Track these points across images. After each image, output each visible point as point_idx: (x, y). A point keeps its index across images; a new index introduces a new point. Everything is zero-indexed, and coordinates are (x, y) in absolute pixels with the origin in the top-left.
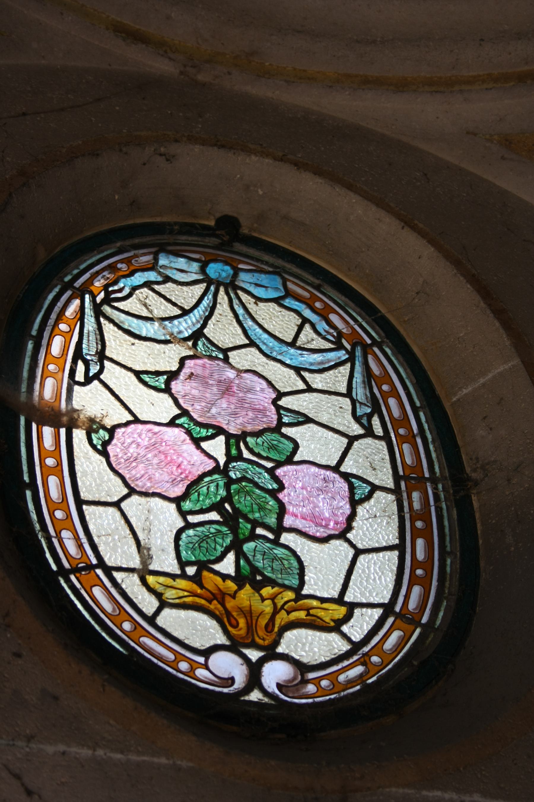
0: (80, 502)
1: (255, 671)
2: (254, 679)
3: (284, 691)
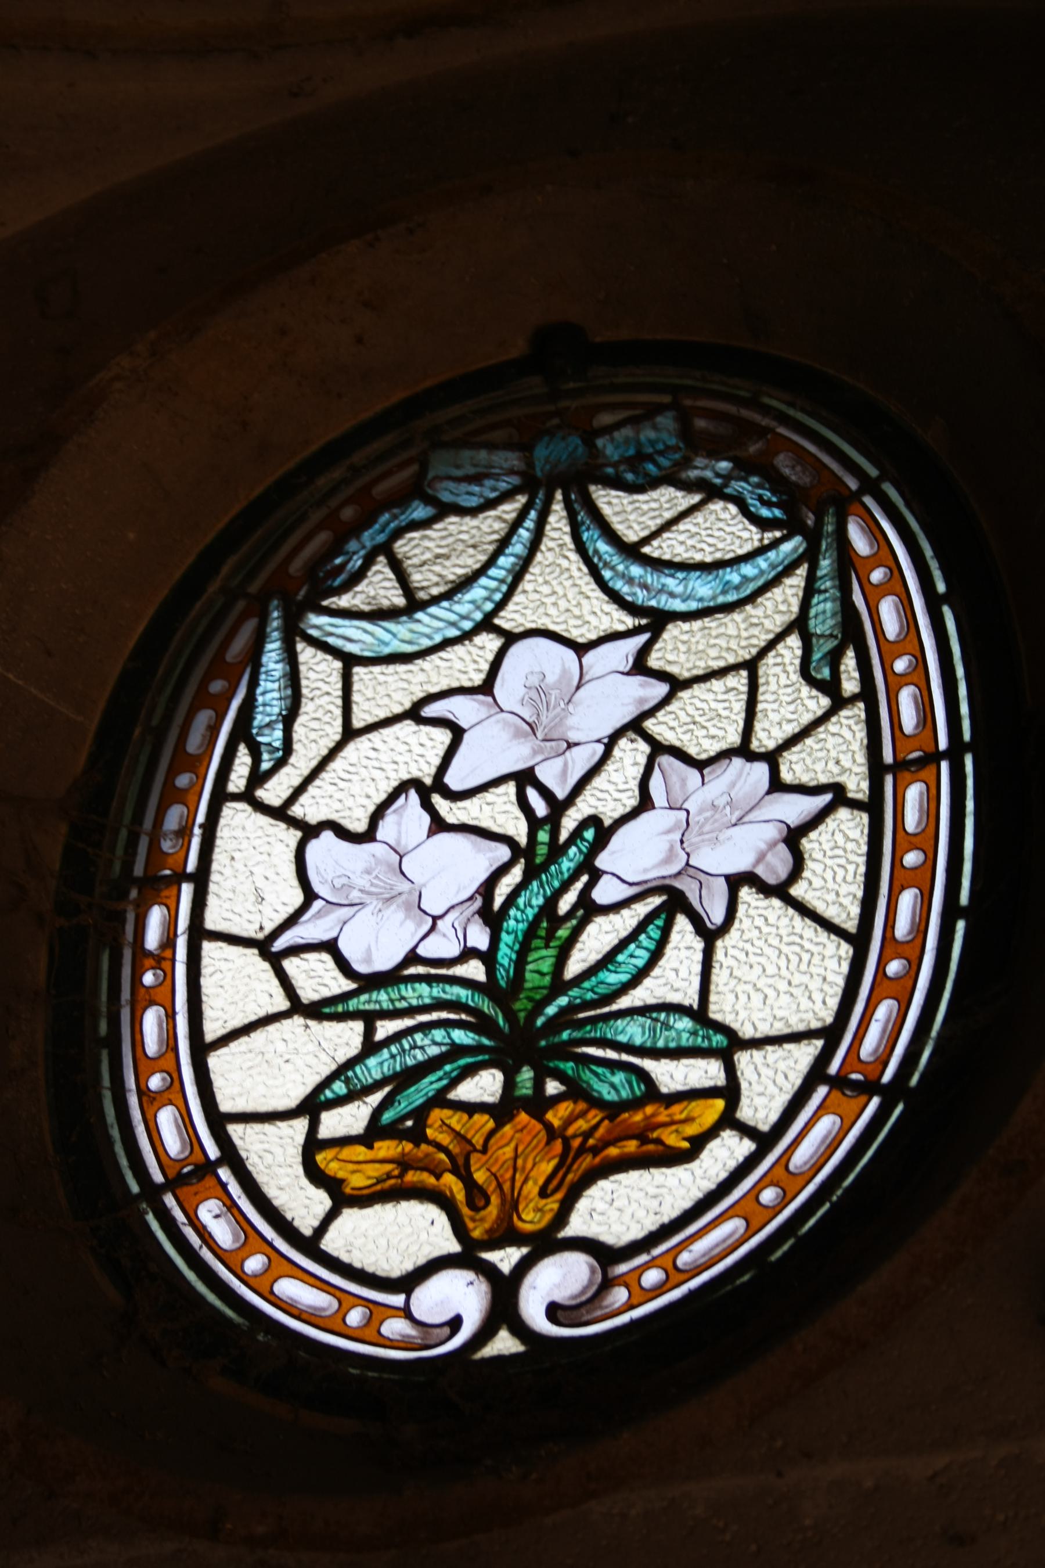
0: (859, 940)
1: (504, 1293)
2: (503, 1308)
3: (562, 1319)
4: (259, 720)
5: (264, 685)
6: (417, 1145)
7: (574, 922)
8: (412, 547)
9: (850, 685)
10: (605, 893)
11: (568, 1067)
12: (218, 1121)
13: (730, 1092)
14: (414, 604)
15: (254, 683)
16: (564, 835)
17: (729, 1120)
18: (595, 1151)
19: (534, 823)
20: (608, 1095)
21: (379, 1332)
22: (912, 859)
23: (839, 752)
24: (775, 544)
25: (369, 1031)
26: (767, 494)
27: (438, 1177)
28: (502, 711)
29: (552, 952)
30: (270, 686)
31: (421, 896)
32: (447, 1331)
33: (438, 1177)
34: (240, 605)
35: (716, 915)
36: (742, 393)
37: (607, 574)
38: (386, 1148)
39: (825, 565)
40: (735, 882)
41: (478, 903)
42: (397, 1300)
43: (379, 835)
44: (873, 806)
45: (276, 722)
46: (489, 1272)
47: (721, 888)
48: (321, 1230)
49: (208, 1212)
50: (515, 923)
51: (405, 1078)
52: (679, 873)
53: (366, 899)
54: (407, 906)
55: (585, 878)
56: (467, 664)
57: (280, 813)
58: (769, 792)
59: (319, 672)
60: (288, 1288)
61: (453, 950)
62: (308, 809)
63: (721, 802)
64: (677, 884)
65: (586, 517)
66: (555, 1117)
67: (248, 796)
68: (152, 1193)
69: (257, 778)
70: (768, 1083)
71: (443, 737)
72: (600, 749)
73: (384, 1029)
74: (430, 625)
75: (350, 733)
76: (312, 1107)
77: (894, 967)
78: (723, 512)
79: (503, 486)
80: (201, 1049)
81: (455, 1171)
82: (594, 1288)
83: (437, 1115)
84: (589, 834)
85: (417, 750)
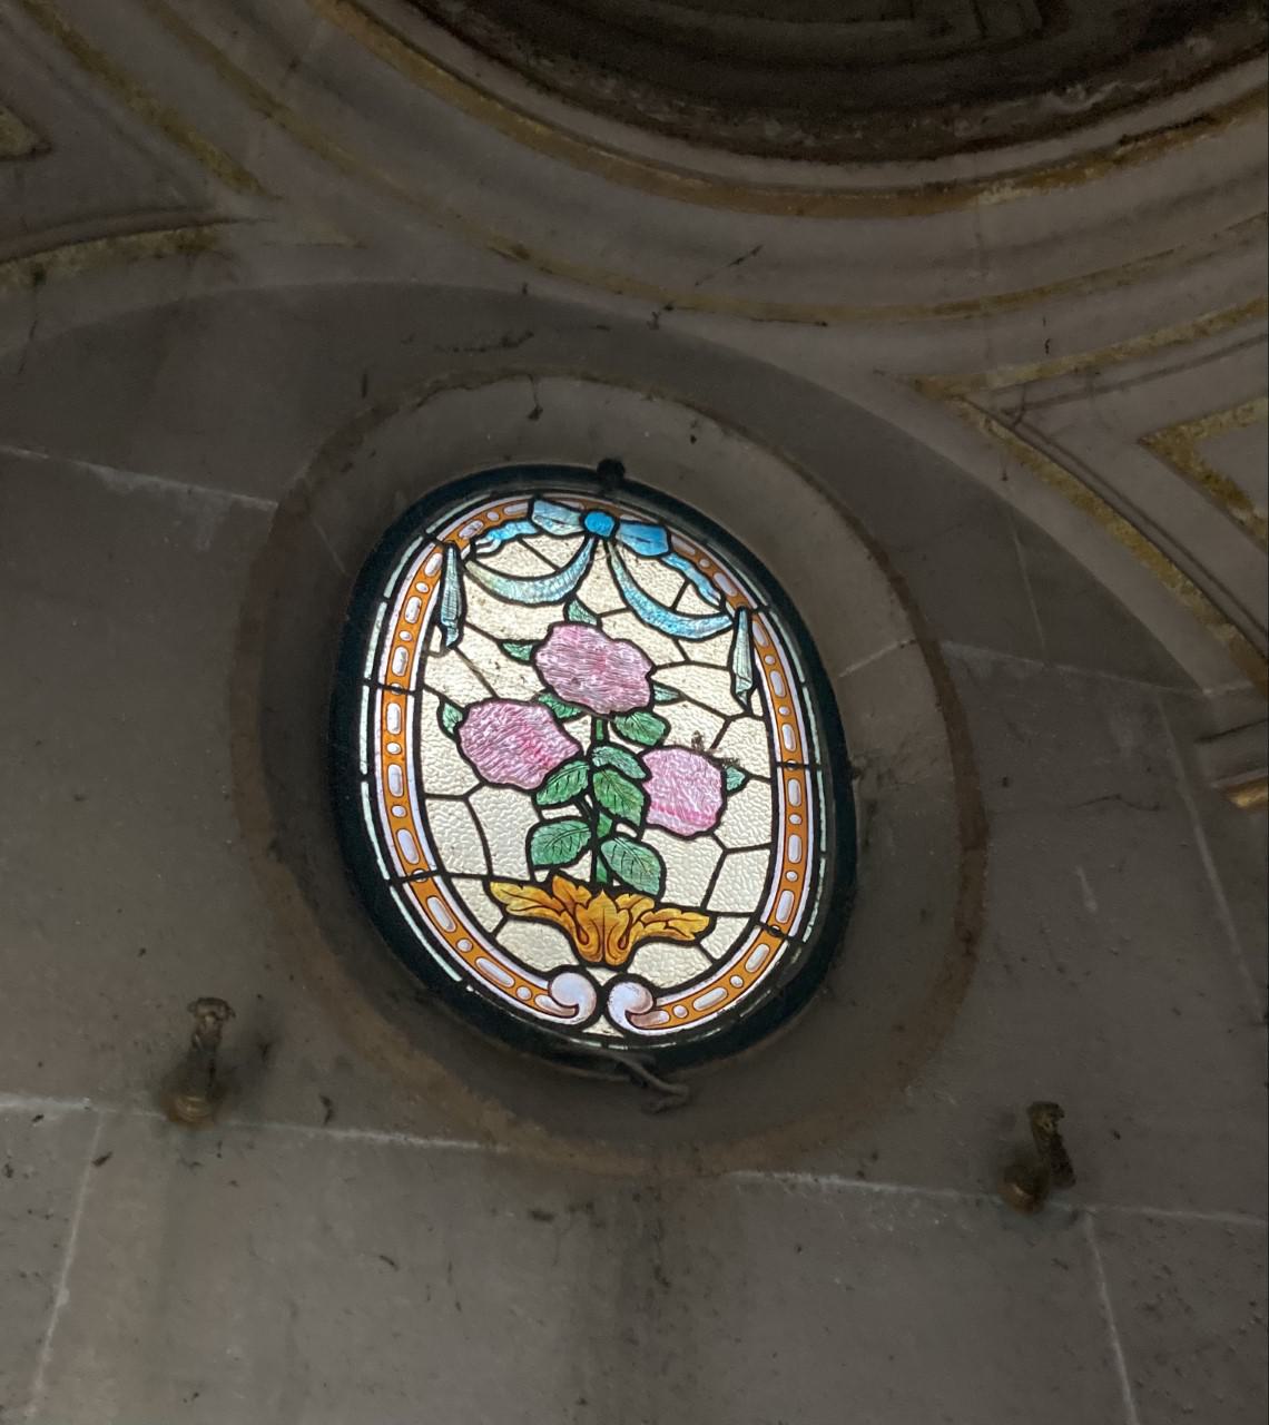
1: (603, 994)
2: (601, 1008)
14: (673, 609)
42: (544, 984)
48: (497, 930)
77: (791, 875)
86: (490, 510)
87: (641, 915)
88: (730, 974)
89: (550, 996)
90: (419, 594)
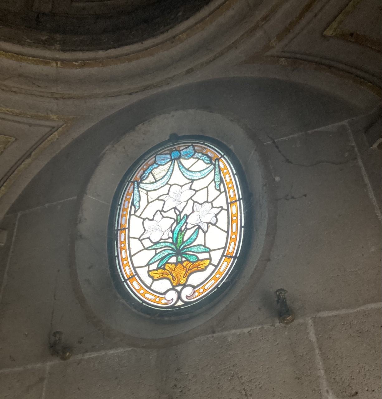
0: (227, 232)
1: (179, 293)
2: (179, 298)
4: (135, 202)
5: (135, 196)
6: (164, 270)
7: (185, 231)
8: (155, 172)
9: (222, 190)
10: (188, 227)
11: (186, 256)
12: (135, 268)
13: (210, 259)
14: (156, 181)
15: (133, 196)
16: (182, 217)
17: (210, 264)
18: (191, 270)
19: (177, 216)
20: (192, 260)
21: (161, 302)
22: (235, 218)
23: (221, 201)
24: (209, 167)
25: (156, 252)
26: (207, 159)
27: (168, 275)
28: (171, 197)
29: (182, 237)
30: (136, 196)
31: (161, 229)
32: (171, 301)
33: (168, 275)
34: (130, 183)
35: (205, 229)
36: (202, 142)
37: (184, 173)
38: (160, 271)
39: (217, 170)
40: (208, 223)
41: (170, 229)
42: (163, 296)
43: (154, 219)
44: (228, 210)
45: (137, 202)
46: (176, 291)
47: (206, 224)
48: (151, 285)
49: (135, 284)
50: (176, 232)
51: (162, 259)
52: (199, 223)
53: (153, 230)
54: (160, 230)
55: (185, 224)
56: (165, 190)
57: (139, 217)
58: (212, 208)
59: (143, 194)
60: (147, 295)
61: (167, 237)
62: (143, 216)
63: (205, 210)
64: (199, 224)
65: (181, 165)
66: (185, 264)
67: (134, 214)
68: (125, 281)
69: (135, 212)
70: (216, 256)
71: (163, 202)
72: (186, 203)
73: (158, 251)
74: (159, 184)
75: (149, 203)
76: (148, 265)
78: (200, 162)
79: (167, 161)
80: (131, 256)
81: (170, 274)
82: (193, 293)
83: (167, 265)
84: (185, 217)
85: (158, 205)
86: (143, 166)
87: (189, 268)
88: (144, 289)
89: (165, 299)
90: (226, 173)
